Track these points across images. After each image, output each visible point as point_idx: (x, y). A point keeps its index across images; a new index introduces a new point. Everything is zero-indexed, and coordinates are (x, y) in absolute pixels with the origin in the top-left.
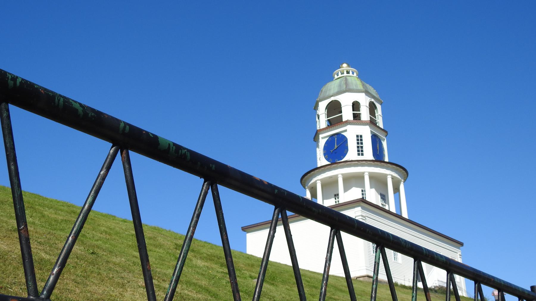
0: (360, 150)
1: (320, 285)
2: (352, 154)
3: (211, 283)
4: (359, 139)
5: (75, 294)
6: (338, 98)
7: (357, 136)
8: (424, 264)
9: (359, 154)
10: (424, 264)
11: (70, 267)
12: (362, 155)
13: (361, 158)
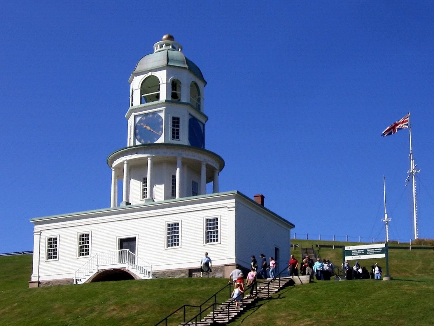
12: (178, 138)
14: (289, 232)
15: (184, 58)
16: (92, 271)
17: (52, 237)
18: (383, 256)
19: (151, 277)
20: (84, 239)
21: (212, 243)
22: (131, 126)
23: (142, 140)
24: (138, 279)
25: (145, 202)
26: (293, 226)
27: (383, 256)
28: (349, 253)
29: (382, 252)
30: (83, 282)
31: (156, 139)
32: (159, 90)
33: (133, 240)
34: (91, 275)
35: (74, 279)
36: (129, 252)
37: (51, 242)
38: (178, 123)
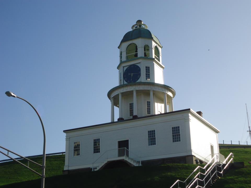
15: (206, 163)
19: (140, 165)
22: (121, 73)
23: (126, 79)
24: (133, 166)
25: (118, 107)
30: (98, 169)
31: (136, 80)
33: (127, 141)
35: (92, 168)
36: (126, 150)
37: (96, 149)
38: (149, 70)
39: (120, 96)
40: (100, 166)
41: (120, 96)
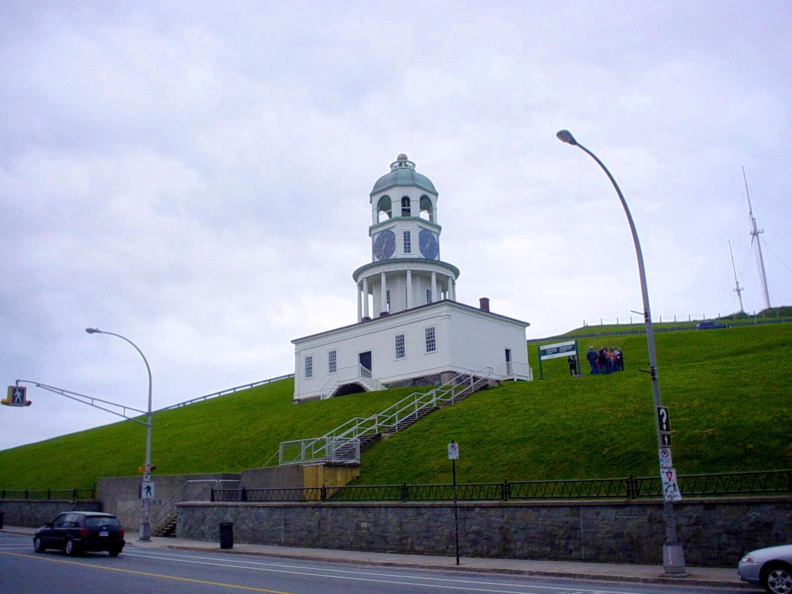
0: (407, 248)
1: (657, 375)
2: (399, 252)
3: (532, 422)
4: (407, 236)
5: (524, 447)
6: (387, 193)
7: (405, 233)
8: (422, 229)
9: (405, 251)
10: (422, 229)
11: (520, 409)
12: (409, 251)
13: (407, 256)
14: (524, 331)
16: (335, 387)
17: (430, 327)
18: (574, 353)
20: (333, 355)
21: (432, 352)
24: (369, 391)
26: (528, 324)
27: (574, 353)
28: (545, 352)
29: (573, 350)
30: (328, 397)
32: (391, 208)
34: (334, 391)
39: (383, 278)
40: (331, 393)
41: (383, 278)
